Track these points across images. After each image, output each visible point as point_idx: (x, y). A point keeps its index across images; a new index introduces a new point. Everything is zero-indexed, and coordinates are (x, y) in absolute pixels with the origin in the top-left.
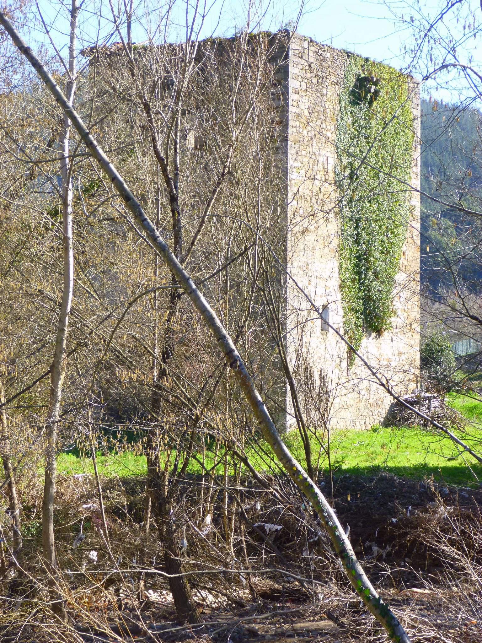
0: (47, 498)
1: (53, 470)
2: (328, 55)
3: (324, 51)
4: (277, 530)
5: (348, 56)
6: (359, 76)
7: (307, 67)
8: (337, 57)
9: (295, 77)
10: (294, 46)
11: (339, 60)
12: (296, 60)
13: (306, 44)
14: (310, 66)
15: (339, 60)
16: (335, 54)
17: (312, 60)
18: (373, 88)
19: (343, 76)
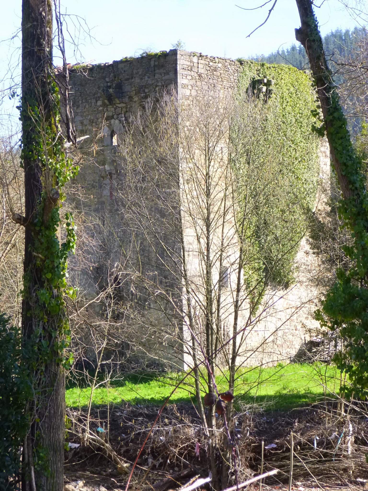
0: (65, 68)
1: (123, 400)
2: (220, 65)
3: (216, 63)
4: (75, 448)
5: (241, 64)
6: (254, 79)
7: (197, 78)
8: (229, 66)
9: (184, 86)
10: (182, 62)
11: (232, 69)
12: (185, 73)
13: (195, 59)
14: (200, 76)
15: (232, 69)
16: (227, 64)
17: (201, 71)
18: (264, 89)
19: (236, 81)
